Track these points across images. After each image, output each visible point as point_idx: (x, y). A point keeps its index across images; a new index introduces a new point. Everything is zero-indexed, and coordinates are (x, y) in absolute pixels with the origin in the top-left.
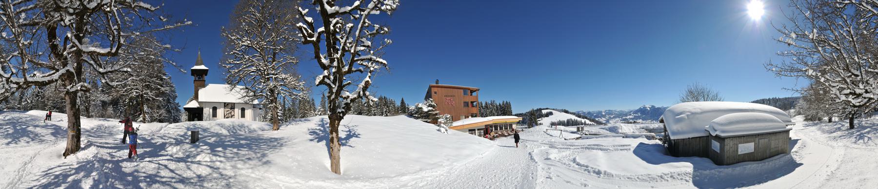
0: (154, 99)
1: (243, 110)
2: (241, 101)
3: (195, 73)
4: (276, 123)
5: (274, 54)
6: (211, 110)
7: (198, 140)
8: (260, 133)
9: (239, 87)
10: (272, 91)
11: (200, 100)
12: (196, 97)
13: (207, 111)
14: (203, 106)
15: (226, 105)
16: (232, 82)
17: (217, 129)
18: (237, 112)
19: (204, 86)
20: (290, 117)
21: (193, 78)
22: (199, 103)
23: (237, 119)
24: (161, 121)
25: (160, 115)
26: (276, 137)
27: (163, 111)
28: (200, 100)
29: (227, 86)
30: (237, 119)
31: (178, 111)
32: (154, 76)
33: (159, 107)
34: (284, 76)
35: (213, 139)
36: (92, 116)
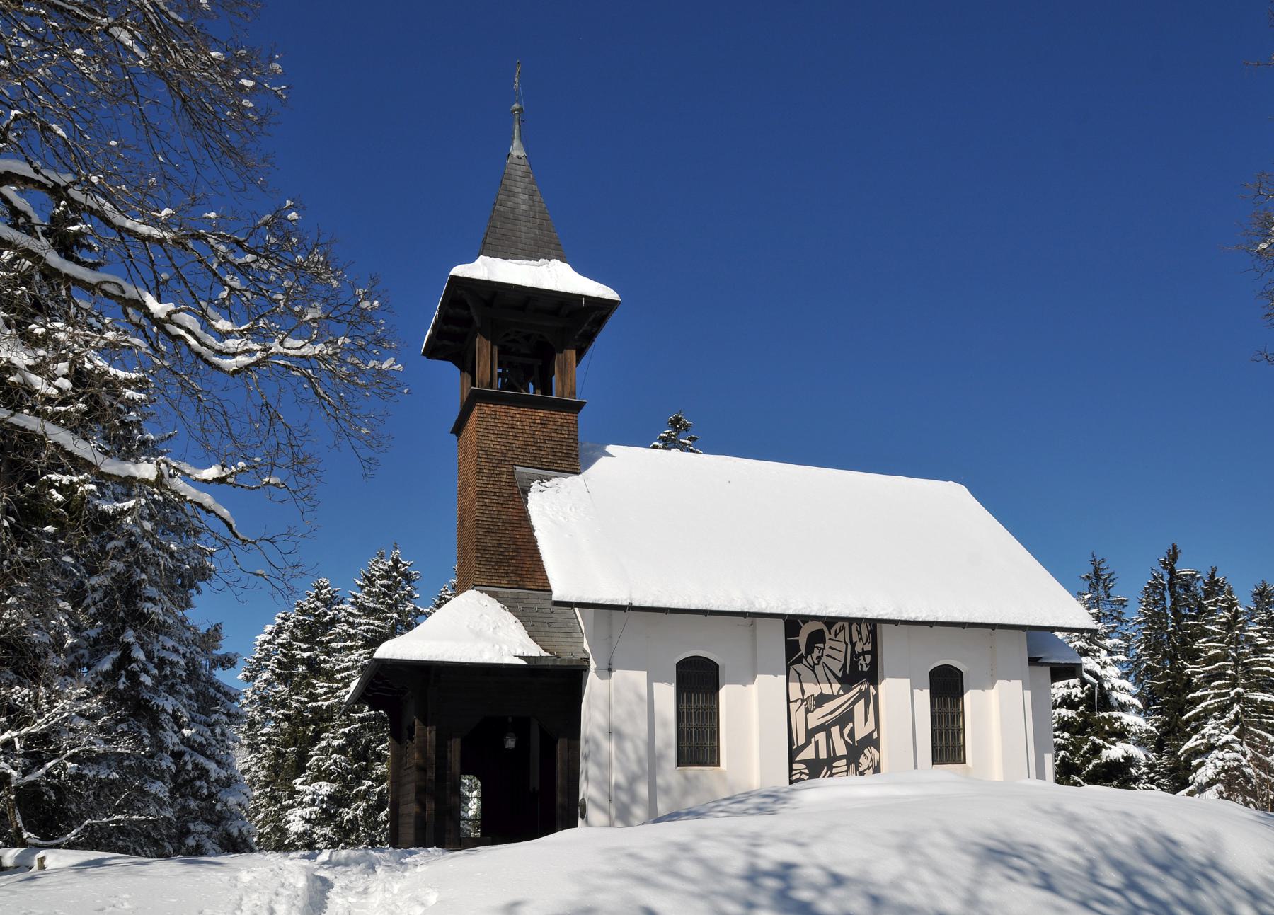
1: (947, 687)
3: (475, 320)
6: (666, 695)
13: (623, 707)
18: (902, 703)
19: (569, 459)
36: (198, 850)
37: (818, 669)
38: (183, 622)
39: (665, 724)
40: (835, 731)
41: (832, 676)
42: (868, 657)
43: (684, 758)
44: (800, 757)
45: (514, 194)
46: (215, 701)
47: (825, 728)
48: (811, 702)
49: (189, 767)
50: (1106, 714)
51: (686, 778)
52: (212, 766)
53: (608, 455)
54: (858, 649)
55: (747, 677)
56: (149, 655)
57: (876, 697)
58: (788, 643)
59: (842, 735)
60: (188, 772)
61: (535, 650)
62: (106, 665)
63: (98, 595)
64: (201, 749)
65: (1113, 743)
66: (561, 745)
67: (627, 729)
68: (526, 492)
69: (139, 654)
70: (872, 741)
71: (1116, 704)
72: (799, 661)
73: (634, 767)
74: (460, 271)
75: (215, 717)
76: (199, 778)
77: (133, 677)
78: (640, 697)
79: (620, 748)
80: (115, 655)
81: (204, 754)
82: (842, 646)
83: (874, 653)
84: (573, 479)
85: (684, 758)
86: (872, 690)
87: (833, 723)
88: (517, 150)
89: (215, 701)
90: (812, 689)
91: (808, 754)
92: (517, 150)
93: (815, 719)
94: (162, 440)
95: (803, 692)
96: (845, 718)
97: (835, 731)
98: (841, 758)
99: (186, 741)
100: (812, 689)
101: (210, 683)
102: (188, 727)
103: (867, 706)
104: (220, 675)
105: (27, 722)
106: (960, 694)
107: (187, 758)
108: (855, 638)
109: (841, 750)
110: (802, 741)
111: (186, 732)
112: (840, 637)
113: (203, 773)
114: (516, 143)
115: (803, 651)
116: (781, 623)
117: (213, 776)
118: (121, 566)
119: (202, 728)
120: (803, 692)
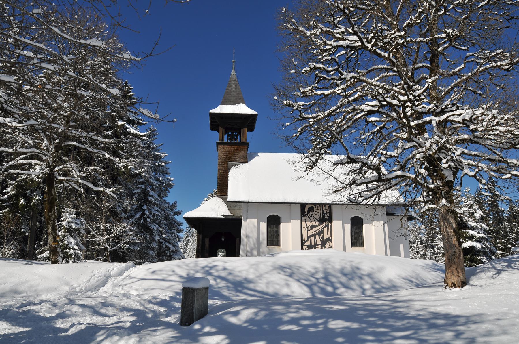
0: (88, 190)
1: (357, 224)
2: (342, 198)
3: (220, 122)
4: (463, 264)
5: (434, 57)
6: (264, 226)
7: (204, 313)
8: (403, 294)
9: (329, 159)
10: (432, 162)
11: (230, 198)
12: (222, 189)
13: (252, 229)
14: (241, 213)
15: (306, 210)
16: (313, 142)
17: (276, 283)
18: (340, 229)
19: (245, 159)
20: (166, 190)
21: (215, 136)
22: (230, 204)
23: (339, 252)
24: (116, 257)
25: (117, 239)
26: (453, 310)
27: (124, 227)
28: (230, 198)
29: (297, 157)
30: (339, 252)
31: (173, 226)
32: (93, 132)
33: (114, 215)
34: (466, 113)
35: (247, 314)
37: (312, 218)
38: (165, 201)
39: (263, 234)
40: (317, 236)
41: (316, 220)
42: (328, 214)
43: (353, 245)
44: (305, 244)
45: (231, 86)
46: (173, 225)
47: (314, 235)
48: (309, 228)
49: (164, 247)
50: (464, 230)
51: (269, 249)
52: (171, 246)
53: (258, 156)
54: (325, 212)
55: (288, 221)
56: (150, 213)
57: (331, 226)
58: (301, 210)
59: (319, 238)
60: (163, 248)
61: (230, 214)
62: (138, 216)
63: (137, 195)
64: (168, 241)
65: (467, 241)
66: (237, 239)
67: (251, 235)
68: (230, 169)
69: (147, 213)
70: (330, 240)
71: (470, 227)
72: (305, 216)
73: (252, 246)
74: (212, 111)
75: (173, 231)
76: (167, 250)
77: (145, 219)
78: (255, 226)
79: (249, 241)
80: (141, 213)
81: (169, 243)
82: (319, 211)
83: (330, 213)
84: (246, 165)
85: (353, 245)
86: (330, 224)
87: (317, 234)
88: (233, 73)
89: (173, 225)
90: (309, 224)
91: (308, 243)
92: (233, 73)
93: (310, 233)
94: (159, 146)
95: (306, 225)
96: (321, 233)
97: (317, 236)
98: (319, 245)
99: (164, 238)
100: (309, 224)
101: (173, 220)
102: (165, 234)
103: (328, 229)
104: (177, 218)
105: (112, 233)
106: (362, 225)
107: (163, 244)
108: (324, 208)
109: (319, 242)
110: (306, 239)
111: (164, 236)
112: (319, 208)
113: (168, 249)
114: (233, 71)
115: (306, 213)
116: (300, 205)
117: (171, 249)
118: (143, 186)
119: (169, 234)
120: (306, 225)
